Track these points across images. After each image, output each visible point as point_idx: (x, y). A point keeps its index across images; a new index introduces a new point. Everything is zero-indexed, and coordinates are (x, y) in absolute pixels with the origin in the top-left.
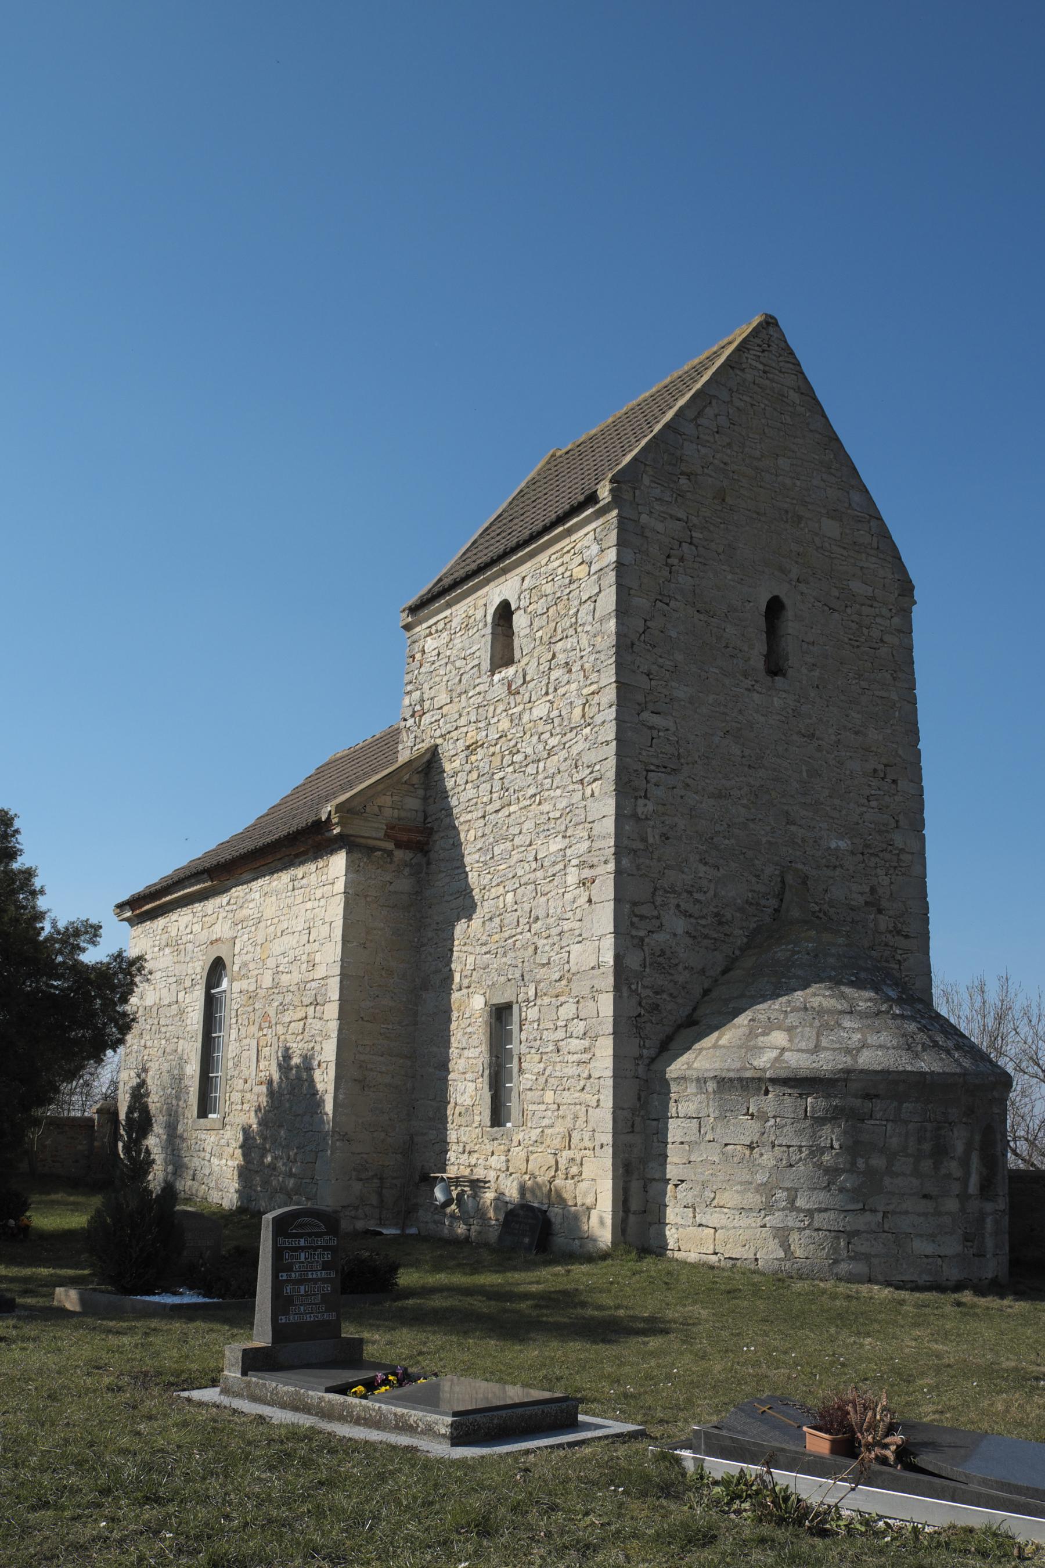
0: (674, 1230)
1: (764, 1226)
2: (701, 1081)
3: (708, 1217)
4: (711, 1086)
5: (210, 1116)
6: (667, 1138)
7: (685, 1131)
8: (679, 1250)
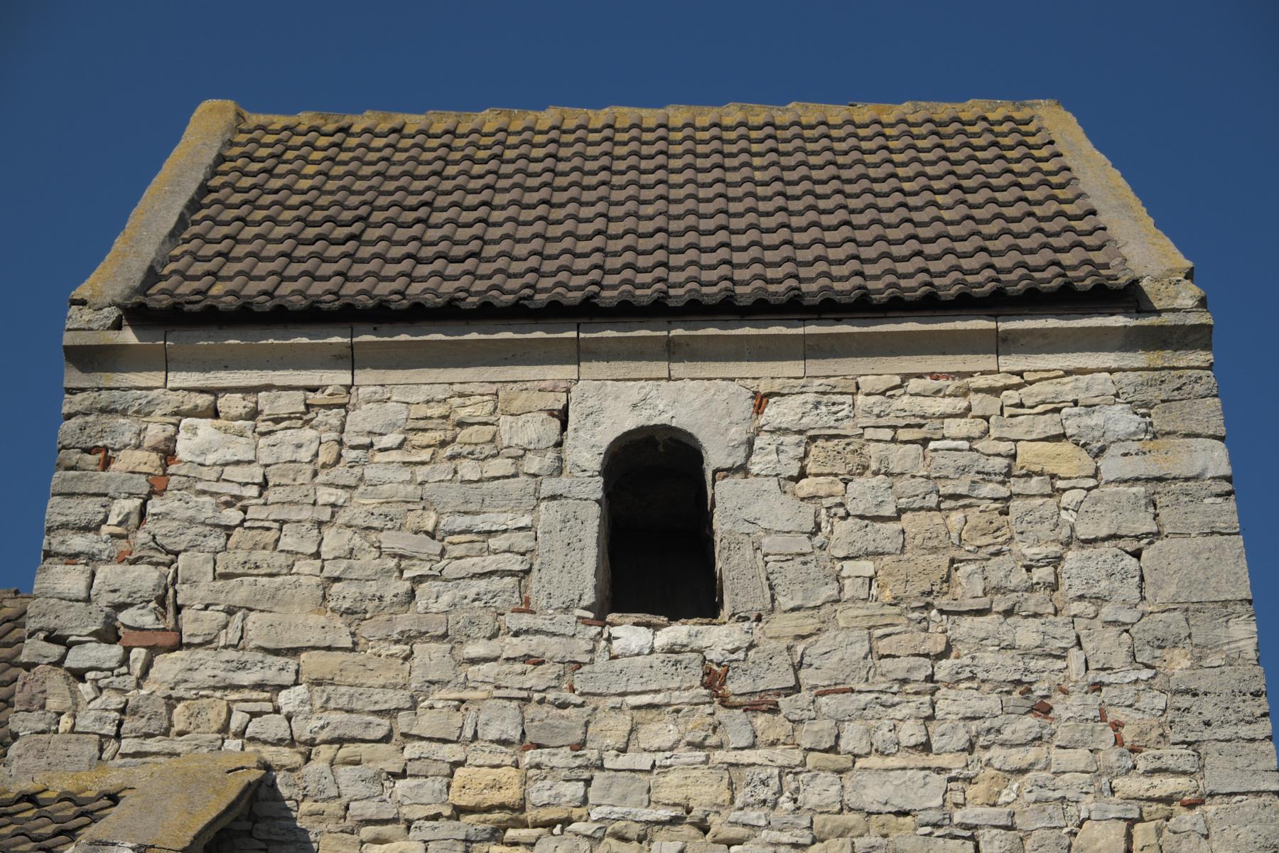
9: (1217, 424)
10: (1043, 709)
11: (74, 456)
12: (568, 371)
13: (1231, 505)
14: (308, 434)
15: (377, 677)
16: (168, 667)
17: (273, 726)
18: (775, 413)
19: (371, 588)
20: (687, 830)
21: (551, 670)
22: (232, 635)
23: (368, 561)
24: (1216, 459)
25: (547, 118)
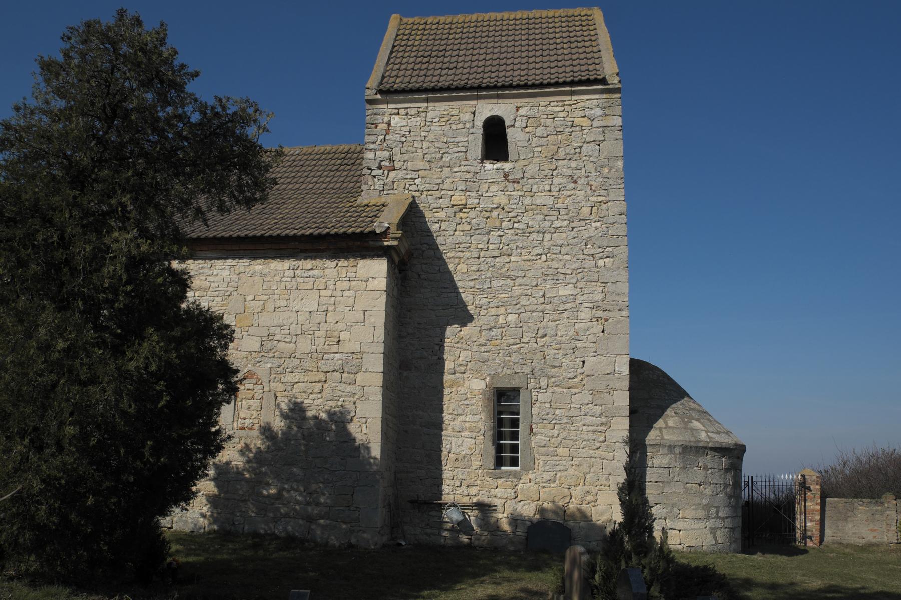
2: (671, 448)
4: (677, 451)
5: (503, 468)
9: (620, 113)
10: (575, 182)
11: (370, 126)
12: (475, 102)
13: (621, 133)
14: (419, 119)
15: (435, 176)
16: (393, 174)
17: (414, 188)
18: (521, 112)
19: (434, 156)
20: (499, 210)
21: (472, 174)
22: (405, 168)
23: (433, 150)
24: (618, 121)
25: (474, 17)
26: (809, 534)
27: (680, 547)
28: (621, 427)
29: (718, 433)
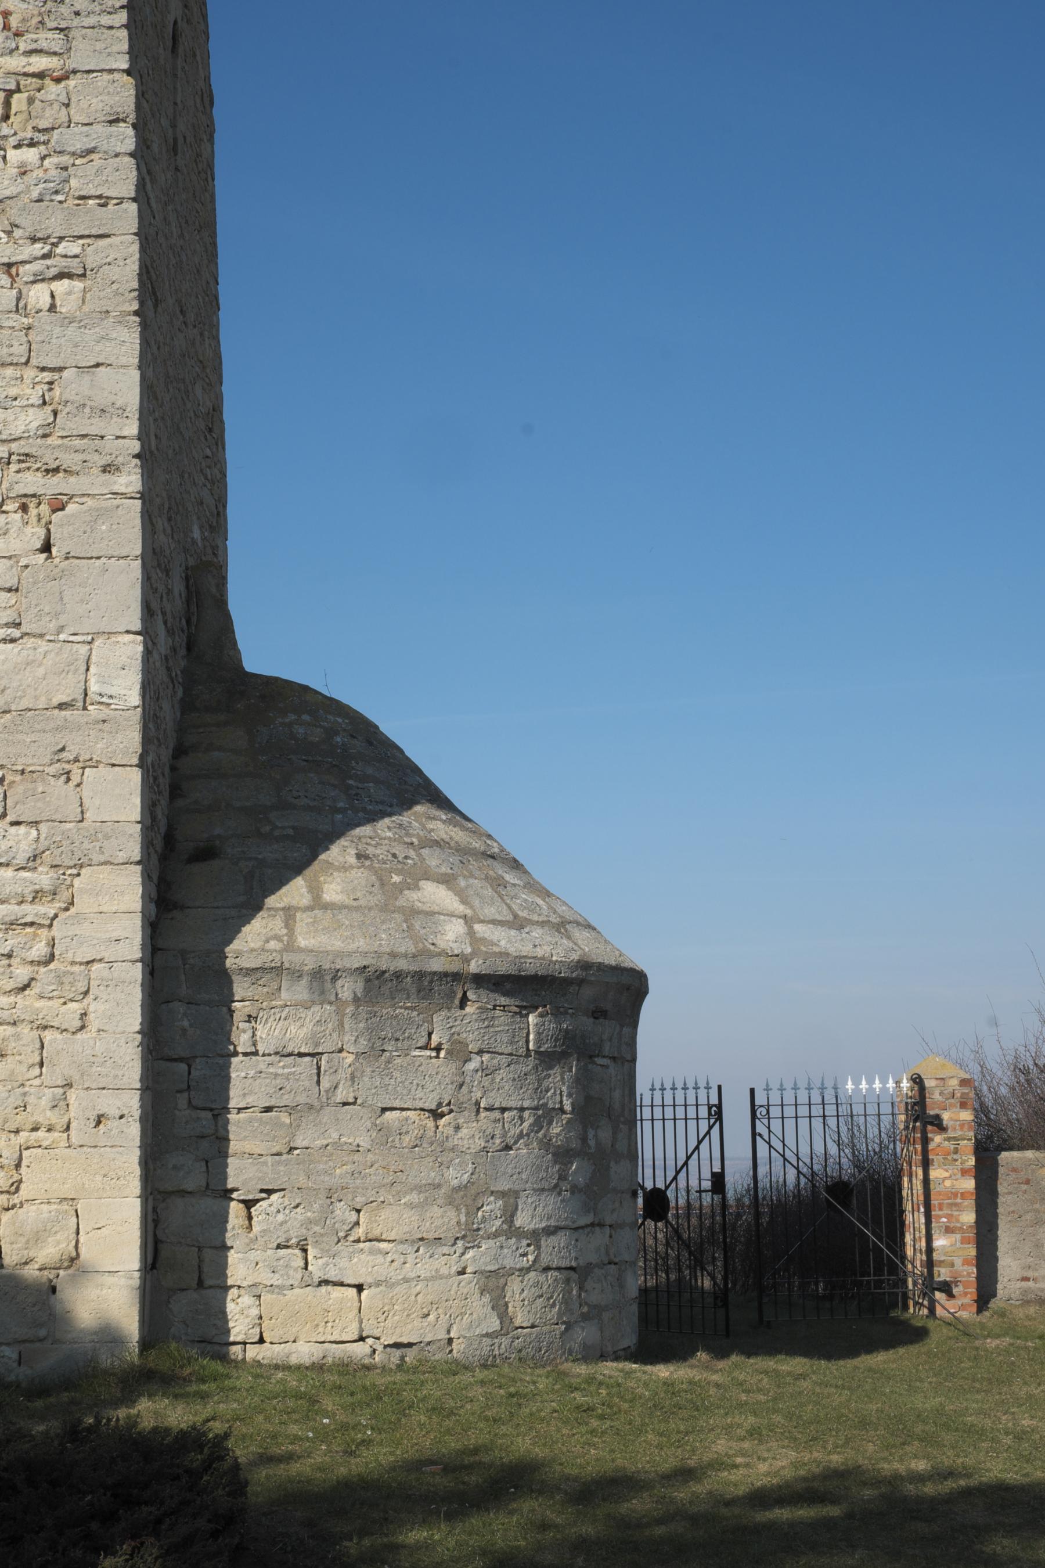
0: (247, 1300)
1: (462, 1272)
2: (322, 979)
3: (343, 1263)
4: (347, 988)
6: (227, 1099)
7: (279, 1081)
8: (261, 1341)
26: (942, 1274)
27: (360, 1350)
28: (112, 909)
29: (518, 923)
